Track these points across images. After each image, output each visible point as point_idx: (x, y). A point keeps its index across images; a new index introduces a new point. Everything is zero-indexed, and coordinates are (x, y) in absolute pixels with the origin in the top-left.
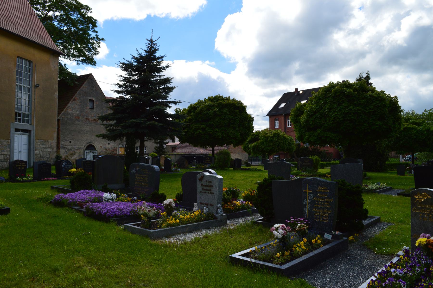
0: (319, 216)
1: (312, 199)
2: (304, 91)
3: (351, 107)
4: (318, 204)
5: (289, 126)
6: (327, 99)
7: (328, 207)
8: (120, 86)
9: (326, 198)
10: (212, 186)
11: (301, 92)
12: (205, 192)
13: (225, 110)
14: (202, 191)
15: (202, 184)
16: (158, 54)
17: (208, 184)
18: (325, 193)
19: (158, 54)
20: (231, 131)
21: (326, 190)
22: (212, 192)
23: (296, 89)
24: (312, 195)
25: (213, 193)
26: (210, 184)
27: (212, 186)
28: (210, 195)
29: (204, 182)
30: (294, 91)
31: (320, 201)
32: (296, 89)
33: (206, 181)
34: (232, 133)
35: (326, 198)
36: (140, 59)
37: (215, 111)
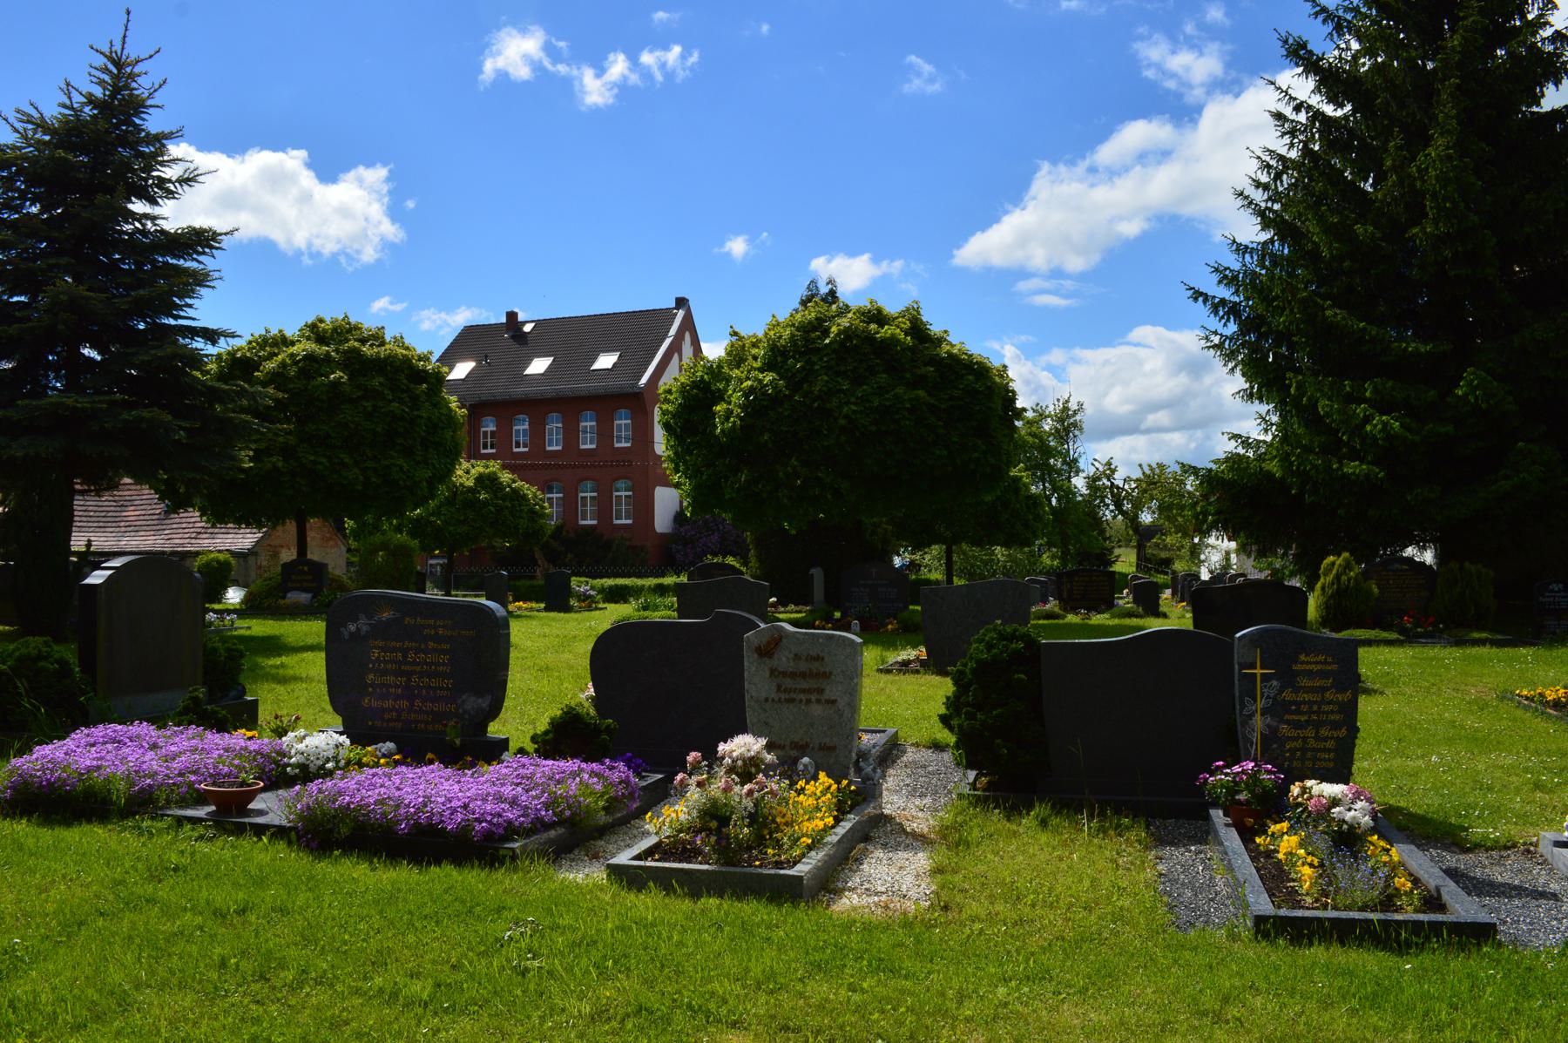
0: (1304, 750)
1: (1274, 698)
2: (539, 323)
3: (900, 390)
4: (1299, 712)
5: (485, 447)
6: (815, 359)
7: (1337, 717)
8: (1228, 278)
9: (1323, 689)
10: (826, 676)
11: (528, 328)
12: (792, 701)
13: (376, 382)
14: (773, 695)
15: (773, 672)
16: (153, 123)
17: (803, 666)
18: (1323, 674)
19: (153, 123)
20: (400, 461)
21: (1325, 663)
22: (827, 695)
23: (512, 316)
24: (1275, 683)
25: (834, 702)
26: (815, 666)
27: (826, 676)
28: (817, 710)
29: (783, 660)
30: (504, 320)
31: (1304, 702)
32: (512, 316)
33: (797, 657)
34: (401, 468)
35: (1327, 689)
36: (70, 133)
37: (337, 382)
